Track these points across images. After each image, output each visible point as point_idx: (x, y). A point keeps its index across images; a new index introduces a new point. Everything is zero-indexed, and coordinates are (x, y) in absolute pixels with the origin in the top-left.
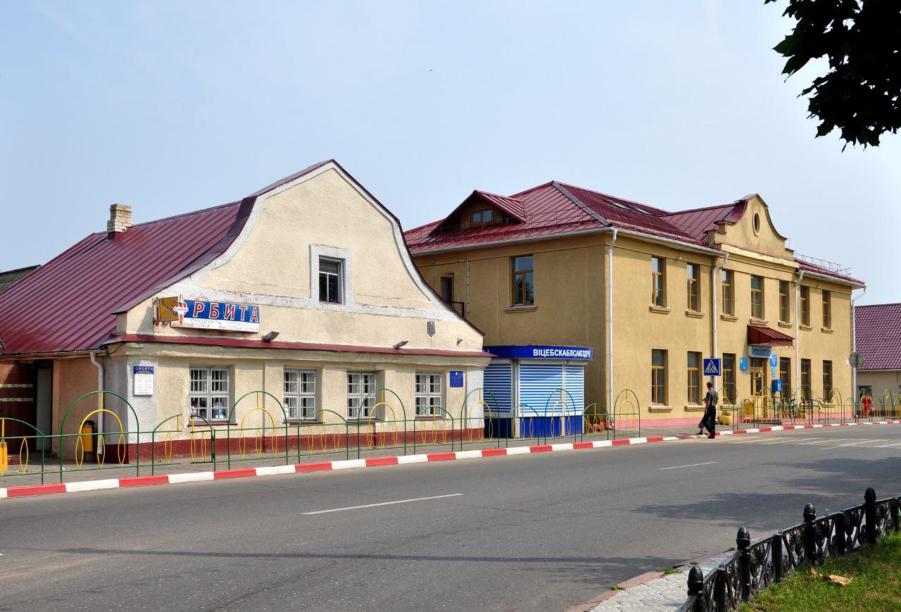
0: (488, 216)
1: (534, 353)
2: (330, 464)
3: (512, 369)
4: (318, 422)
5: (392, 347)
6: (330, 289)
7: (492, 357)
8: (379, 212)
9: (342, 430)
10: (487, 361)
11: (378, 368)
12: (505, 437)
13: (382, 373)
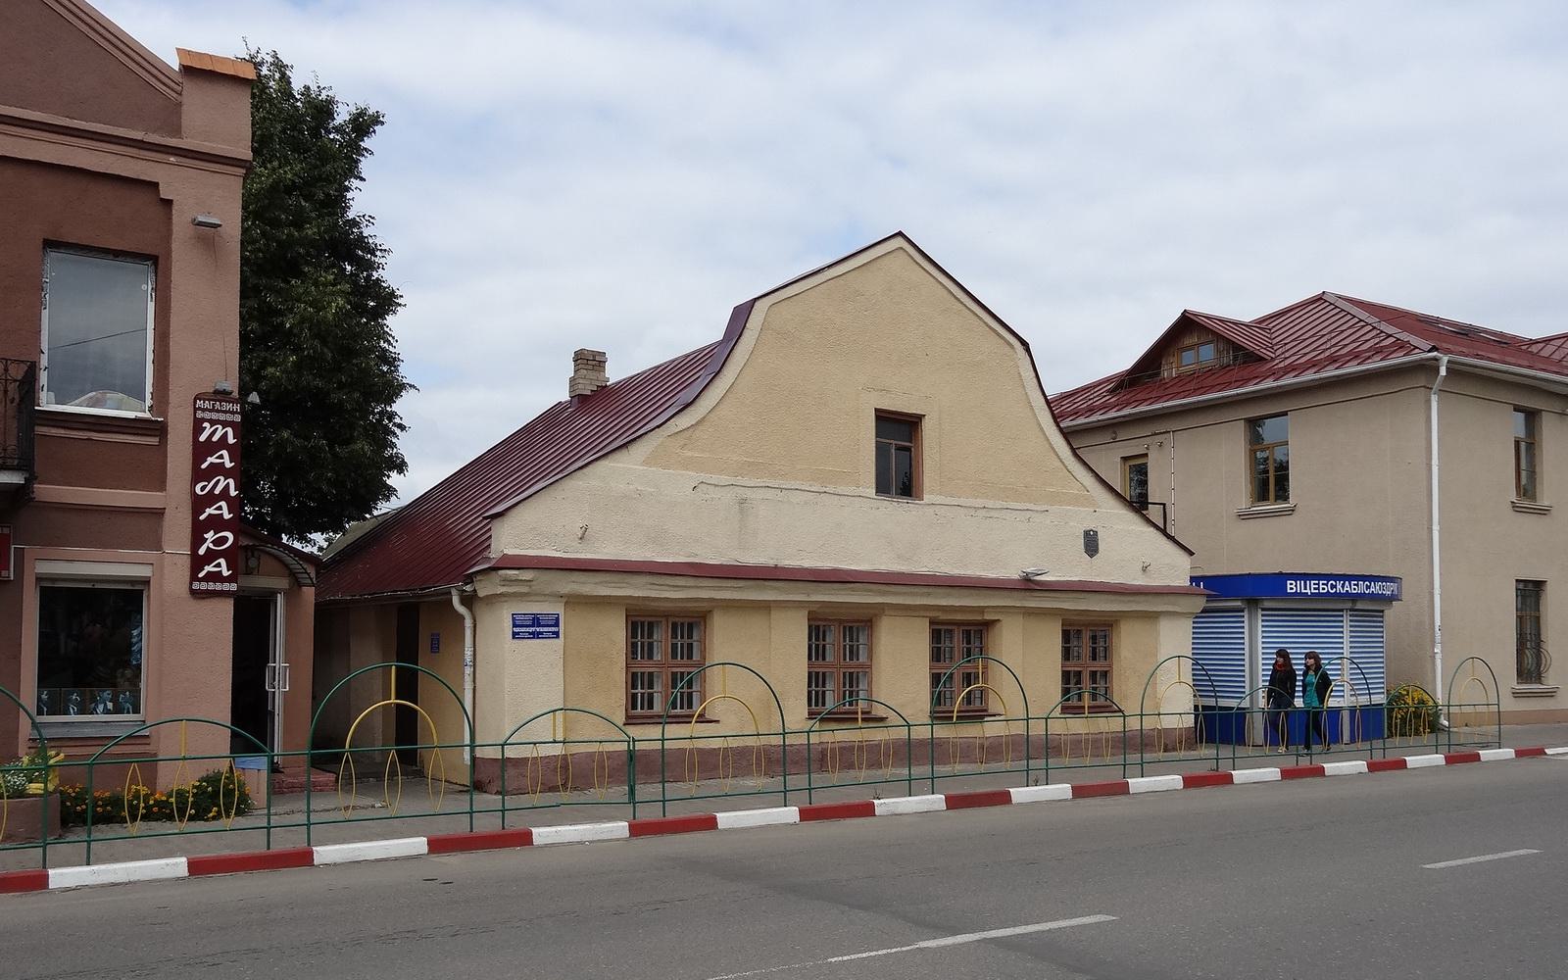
0: (1208, 354)
1: (1289, 586)
2: (530, 834)
3: (1246, 619)
5: (1017, 577)
7: (1208, 596)
8: (990, 327)
10: (1200, 603)
12: (1380, 736)
13: (998, 625)
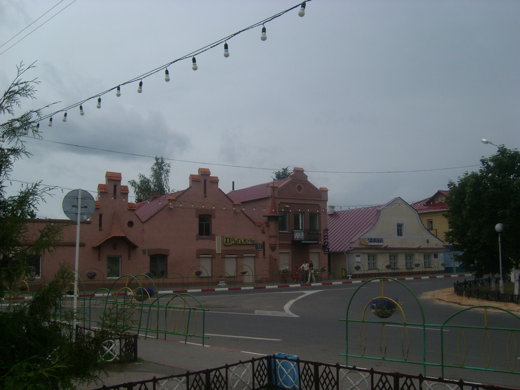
4: (397, 269)
6: (400, 233)
9: (405, 270)
11: (414, 253)
